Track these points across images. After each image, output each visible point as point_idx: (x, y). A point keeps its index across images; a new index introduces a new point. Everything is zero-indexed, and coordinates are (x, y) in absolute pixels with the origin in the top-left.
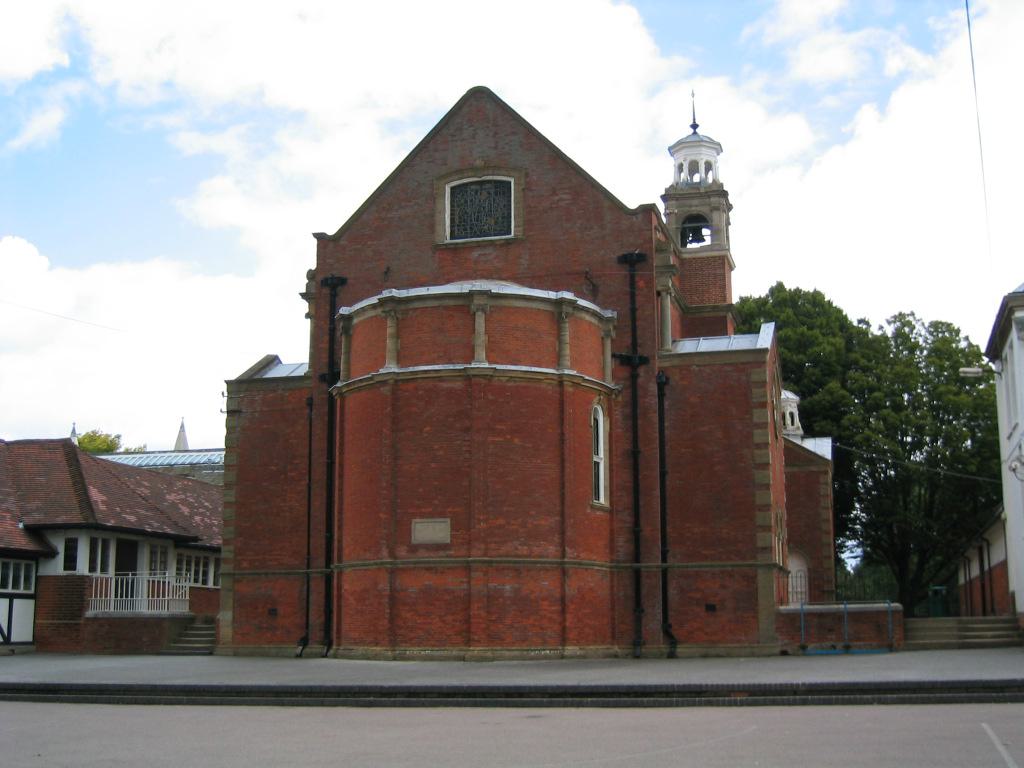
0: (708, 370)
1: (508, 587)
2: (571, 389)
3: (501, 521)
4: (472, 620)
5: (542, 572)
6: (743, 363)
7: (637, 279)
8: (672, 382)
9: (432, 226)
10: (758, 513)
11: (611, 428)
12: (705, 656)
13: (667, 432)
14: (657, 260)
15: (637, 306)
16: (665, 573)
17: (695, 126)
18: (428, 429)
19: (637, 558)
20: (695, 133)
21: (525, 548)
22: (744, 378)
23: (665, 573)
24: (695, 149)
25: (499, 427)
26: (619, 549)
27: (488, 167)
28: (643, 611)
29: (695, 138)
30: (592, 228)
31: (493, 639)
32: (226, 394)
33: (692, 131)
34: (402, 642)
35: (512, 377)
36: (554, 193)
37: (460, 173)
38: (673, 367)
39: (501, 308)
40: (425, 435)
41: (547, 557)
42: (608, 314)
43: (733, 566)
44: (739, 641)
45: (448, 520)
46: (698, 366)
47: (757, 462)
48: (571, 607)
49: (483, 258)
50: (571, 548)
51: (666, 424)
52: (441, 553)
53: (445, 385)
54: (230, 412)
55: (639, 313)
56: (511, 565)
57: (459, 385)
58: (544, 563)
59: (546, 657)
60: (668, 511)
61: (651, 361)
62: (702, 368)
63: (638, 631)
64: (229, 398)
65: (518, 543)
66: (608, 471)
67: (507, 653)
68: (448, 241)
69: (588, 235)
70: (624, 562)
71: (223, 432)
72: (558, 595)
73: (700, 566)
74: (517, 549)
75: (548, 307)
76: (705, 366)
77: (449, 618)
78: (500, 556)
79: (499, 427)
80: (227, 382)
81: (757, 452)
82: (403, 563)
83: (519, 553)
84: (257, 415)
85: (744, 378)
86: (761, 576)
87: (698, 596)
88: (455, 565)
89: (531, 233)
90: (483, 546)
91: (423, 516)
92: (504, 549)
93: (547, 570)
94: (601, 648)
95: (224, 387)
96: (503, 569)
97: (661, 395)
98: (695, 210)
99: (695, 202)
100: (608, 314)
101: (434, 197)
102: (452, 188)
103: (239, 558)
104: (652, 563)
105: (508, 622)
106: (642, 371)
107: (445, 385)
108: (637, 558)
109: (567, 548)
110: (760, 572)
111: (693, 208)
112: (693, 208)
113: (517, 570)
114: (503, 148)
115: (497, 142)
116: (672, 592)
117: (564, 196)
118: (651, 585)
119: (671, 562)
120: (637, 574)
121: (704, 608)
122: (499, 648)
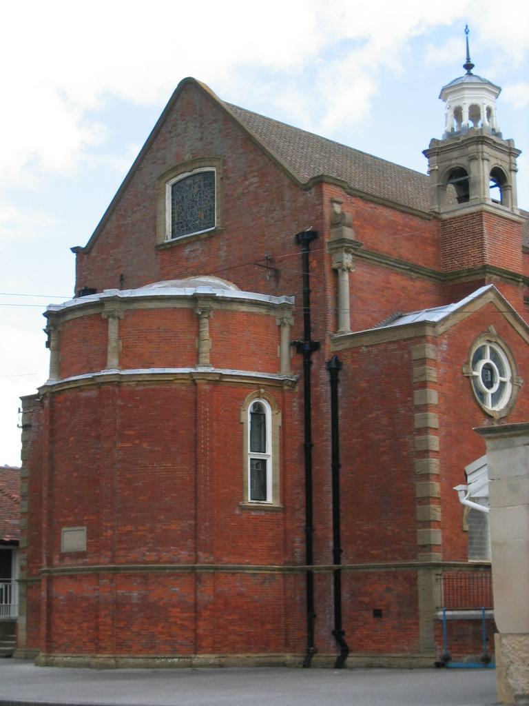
0: (374, 350)
1: (135, 594)
2: (207, 387)
3: (129, 528)
4: (101, 628)
5: (172, 578)
6: (405, 340)
7: (311, 259)
8: (344, 367)
9: (154, 223)
10: (418, 507)
11: (283, 422)
12: (370, 666)
13: (340, 422)
14: (328, 237)
15: (311, 289)
16: (337, 574)
17: (469, 66)
18: (72, 439)
19: (309, 559)
20: (470, 74)
21: (155, 554)
22: (406, 356)
23: (337, 574)
24: (458, 94)
25: (127, 432)
26: (297, 550)
27: (197, 160)
28: (315, 616)
29: (468, 80)
30: (274, 210)
31: (121, 646)
32: (21, 410)
33: (466, 71)
34: (56, 648)
35: (141, 381)
36: (245, 179)
37: (175, 169)
38: (346, 350)
39: (136, 311)
40: (71, 445)
41: (179, 562)
42: (281, 300)
43: (396, 566)
44: (402, 651)
45: (85, 528)
46: (367, 346)
47: (418, 449)
48: (206, 614)
49: (193, 255)
50: (205, 552)
51: (340, 413)
52: (80, 561)
53: (84, 394)
54: (25, 427)
55: (312, 296)
56: (139, 571)
57: (93, 393)
58: (175, 568)
59: (172, 666)
60: (341, 507)
61: (322, 347)
62: (370, 348)
63: (311, 642)
64: (24, 413)
65: (146, 549)
66: (278, 469)
67: (132, 661)
68: (170, 240)
69: (272, 218)
70: (300, 564)
71: (18, 446)
72: (191, 601)
73: (368, 567)
74: (144, 555)
75: (186, 305)
76: (372, 346)
77: (85, 625)
78: (127, 562)
79: (127, 432)
80: (22, 398)
81: (418, 438)
82: (58, 571)
83: (147, 559)
84: (41, 428)
85: (406, 356)
86: (422, 577)
87: (367, 599)
88: (90, 572)
89: (228, 223)
90: (109, 553)
91: (68, 524)
92: (132, 556)
93: (178, 575)
94: (254, 657)
95: (20, 404)
96: (130, 576)
97: (334, 383)
98: (455, 163)
99: (455, 154)
100: (281, 300)
101: (158, 196)
102: (173, 186)
103: (31, 565)
104: (324, 563)
105: (135, 629)
106: (314, 358)
107: (84, 394)
108: (309, 559)
109: (199, 553)
110: (420, 572)
111: (453, 162)
112: (453, 162)
113: (143, 576)
114: (207, 138)
115: (202, 133)
116: (345, 595)
117: (254, 180)
118: (325, 587)
119: (345, 563)
120: (310, 576)
121: (372, 612)
122: (127, 655)
